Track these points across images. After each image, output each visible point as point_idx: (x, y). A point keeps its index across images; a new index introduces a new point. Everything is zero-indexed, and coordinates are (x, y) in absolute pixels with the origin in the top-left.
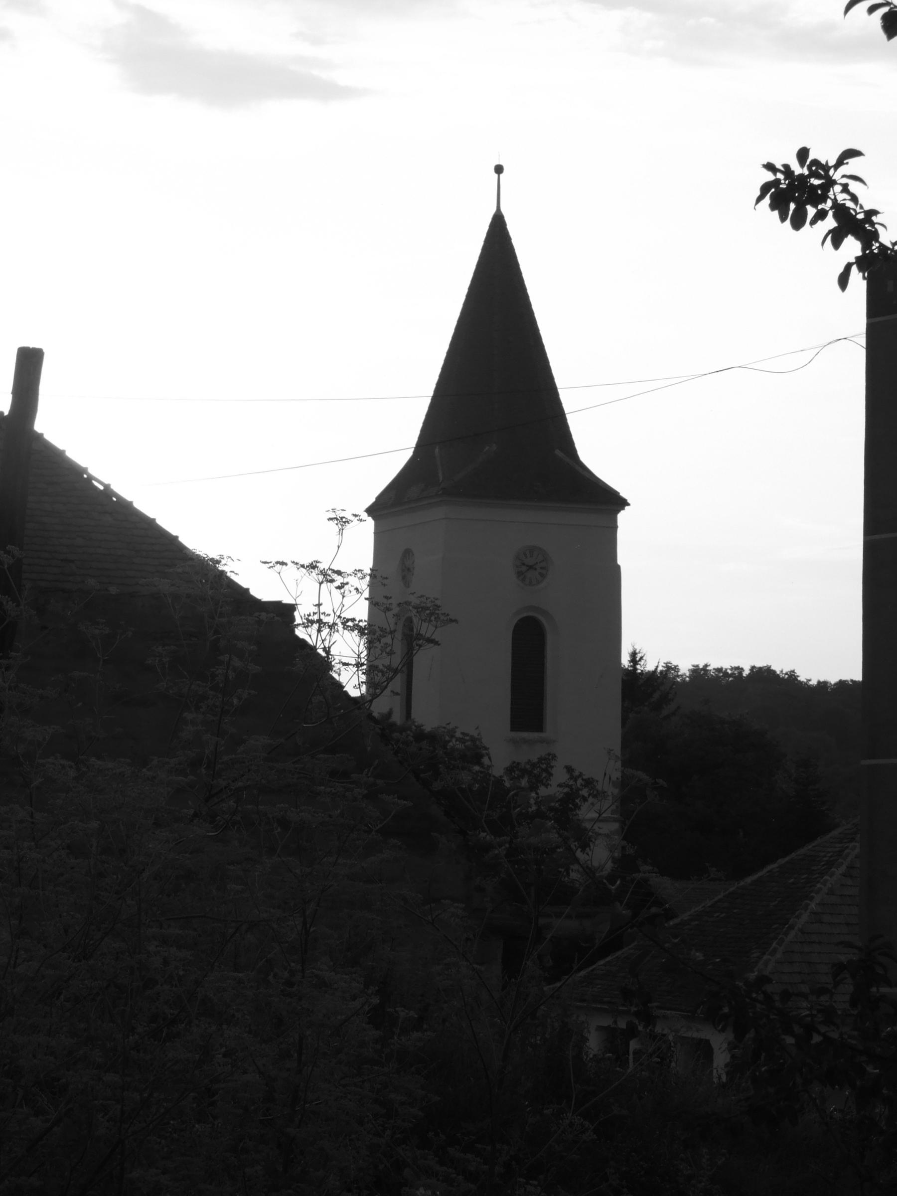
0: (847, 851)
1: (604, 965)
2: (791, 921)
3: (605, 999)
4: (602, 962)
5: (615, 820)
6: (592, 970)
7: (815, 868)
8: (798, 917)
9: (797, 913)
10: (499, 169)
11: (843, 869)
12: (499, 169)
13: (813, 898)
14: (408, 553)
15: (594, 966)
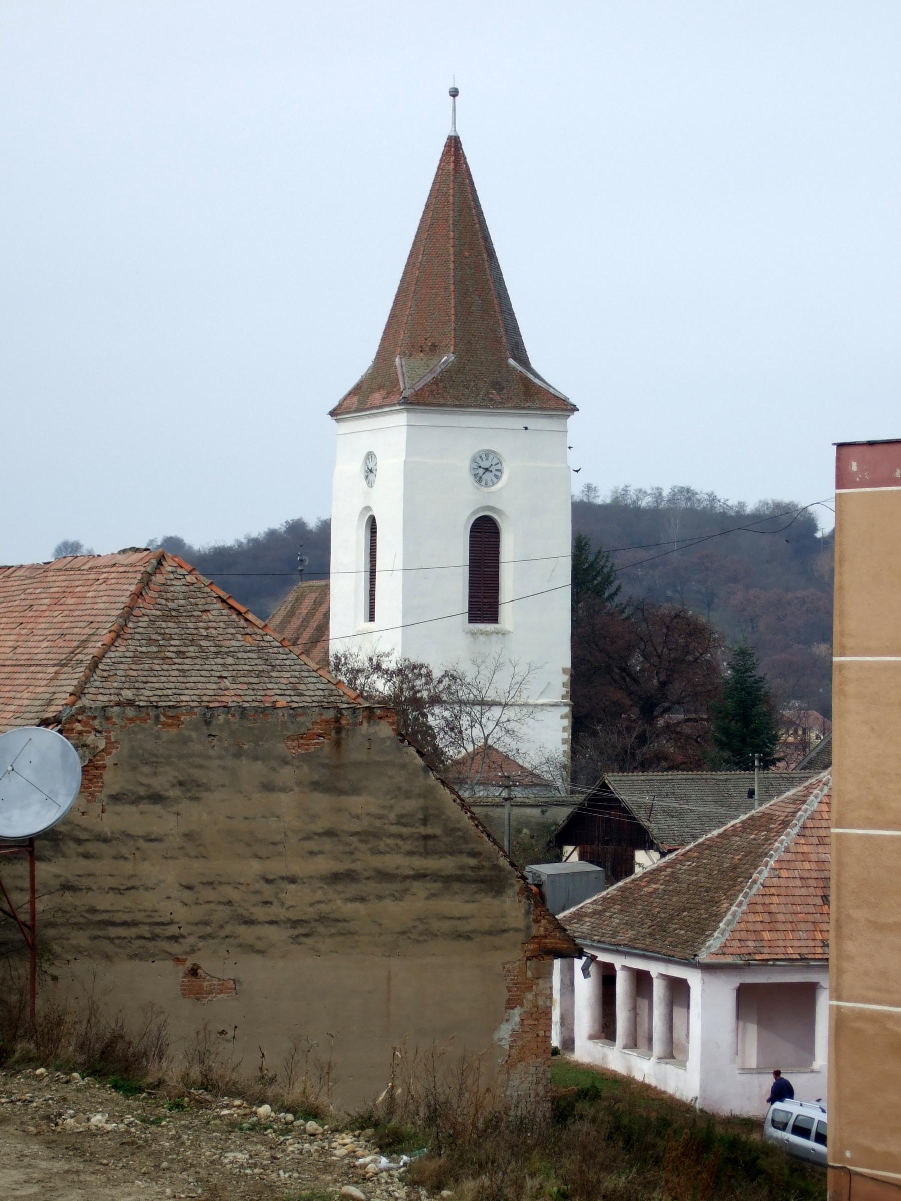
0: (800, 813)
1: (591, 903)
2: (754, 876)
3: (595, 938)
4: (589, 901)
5: (565, 705)
6: (581, 908)
7: (772, 826)
8: (760, 873)
9: (759, 869)
10: (454, 93)
11: (796, 830)
12: (454, 93)
13: (771, 856)
14: (370, 456)
15: (582, 905)
